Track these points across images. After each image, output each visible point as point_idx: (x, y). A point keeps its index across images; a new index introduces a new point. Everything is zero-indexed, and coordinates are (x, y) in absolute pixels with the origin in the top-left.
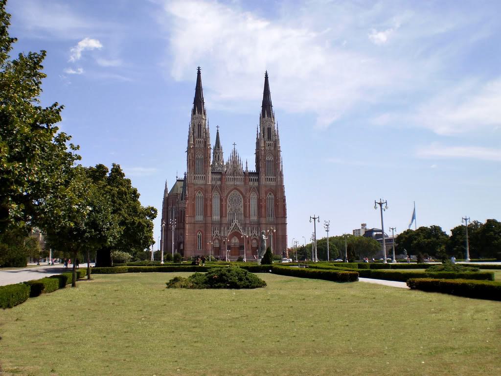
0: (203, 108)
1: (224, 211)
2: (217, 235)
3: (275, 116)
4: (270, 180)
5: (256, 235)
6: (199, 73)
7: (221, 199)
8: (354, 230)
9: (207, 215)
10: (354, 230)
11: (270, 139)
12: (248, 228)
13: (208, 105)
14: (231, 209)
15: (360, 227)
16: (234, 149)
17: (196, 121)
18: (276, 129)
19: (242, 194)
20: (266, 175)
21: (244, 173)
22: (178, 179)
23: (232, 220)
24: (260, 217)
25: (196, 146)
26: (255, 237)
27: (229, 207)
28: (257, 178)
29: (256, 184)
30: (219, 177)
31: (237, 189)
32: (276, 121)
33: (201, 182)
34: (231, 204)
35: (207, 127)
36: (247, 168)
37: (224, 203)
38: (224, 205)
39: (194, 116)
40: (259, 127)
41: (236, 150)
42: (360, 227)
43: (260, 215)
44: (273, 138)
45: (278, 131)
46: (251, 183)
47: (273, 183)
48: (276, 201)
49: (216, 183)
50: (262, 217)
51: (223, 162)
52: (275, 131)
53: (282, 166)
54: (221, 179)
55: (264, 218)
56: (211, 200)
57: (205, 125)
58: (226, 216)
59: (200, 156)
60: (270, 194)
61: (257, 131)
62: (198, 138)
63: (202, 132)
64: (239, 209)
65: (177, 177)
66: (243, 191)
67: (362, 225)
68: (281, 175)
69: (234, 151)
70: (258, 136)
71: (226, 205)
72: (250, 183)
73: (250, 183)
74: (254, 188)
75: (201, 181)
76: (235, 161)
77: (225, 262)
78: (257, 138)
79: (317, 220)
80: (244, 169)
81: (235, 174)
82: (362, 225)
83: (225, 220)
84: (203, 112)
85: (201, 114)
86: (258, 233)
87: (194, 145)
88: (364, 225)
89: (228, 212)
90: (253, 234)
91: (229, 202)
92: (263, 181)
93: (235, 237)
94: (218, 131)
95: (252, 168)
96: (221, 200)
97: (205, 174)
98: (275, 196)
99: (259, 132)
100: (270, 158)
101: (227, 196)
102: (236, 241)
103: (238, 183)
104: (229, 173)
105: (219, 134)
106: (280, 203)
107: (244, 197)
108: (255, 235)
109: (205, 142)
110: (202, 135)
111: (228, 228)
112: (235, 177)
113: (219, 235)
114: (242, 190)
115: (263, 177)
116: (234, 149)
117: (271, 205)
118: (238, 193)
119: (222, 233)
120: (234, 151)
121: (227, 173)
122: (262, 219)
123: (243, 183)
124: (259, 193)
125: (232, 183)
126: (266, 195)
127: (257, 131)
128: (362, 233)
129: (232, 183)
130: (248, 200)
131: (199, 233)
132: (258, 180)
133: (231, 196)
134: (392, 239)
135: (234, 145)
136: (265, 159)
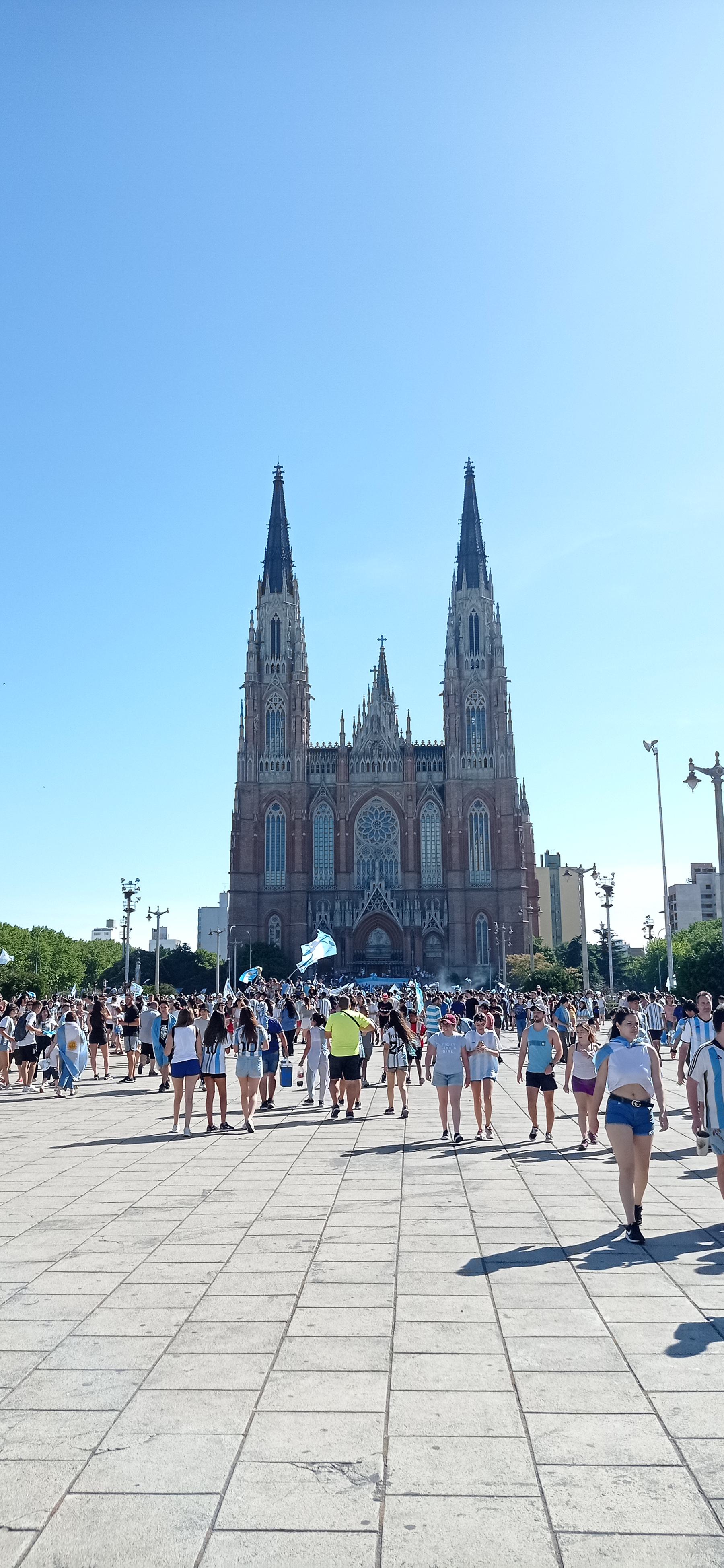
0: (482, 576)
3: (494, 582)
5: (438, 922)
6: (278, 482)
9: (293, 868)
10: (200, 910)
14: (365, 851)
17: (269, 611)
24: (447, 871)
26: (432, 929)
27: (359, 843)
36: (409, 732)
37: (343, 834)
39: (459, 592)
40: (255, 612)
44: (484, 644)
46: (423, 776)
47: (486, 773)
49: (430, 777)
50: (451, 870)
55: (458, 873)
62: (273, 656)
63: (283, 641)
66: (397, 799)
68: (509, 748)
72: (418, 774)
84: (482, 581)
85: (477, 586)
86: (442, 917)
90: (427, 920)
93: (378, 929)
97: (491, 751)
98: (493, 808)
101: (353, 814)
102: (382, 942)
103: (384, 776)
106: (504, 829)
107: (402, 815)
108: (433, 922)
109: (291, 668)
110: (282, 647)
111: (355, 905)
118: (384, 803)
119: (337, 917)
122: (451, 875)
123: (398, 776)
124: (443, 799)
125: (368, 776)
129: (368, 776)
131: (482, 917)
132: (443, 768)
133: (365, 813)
136: (462, 704)
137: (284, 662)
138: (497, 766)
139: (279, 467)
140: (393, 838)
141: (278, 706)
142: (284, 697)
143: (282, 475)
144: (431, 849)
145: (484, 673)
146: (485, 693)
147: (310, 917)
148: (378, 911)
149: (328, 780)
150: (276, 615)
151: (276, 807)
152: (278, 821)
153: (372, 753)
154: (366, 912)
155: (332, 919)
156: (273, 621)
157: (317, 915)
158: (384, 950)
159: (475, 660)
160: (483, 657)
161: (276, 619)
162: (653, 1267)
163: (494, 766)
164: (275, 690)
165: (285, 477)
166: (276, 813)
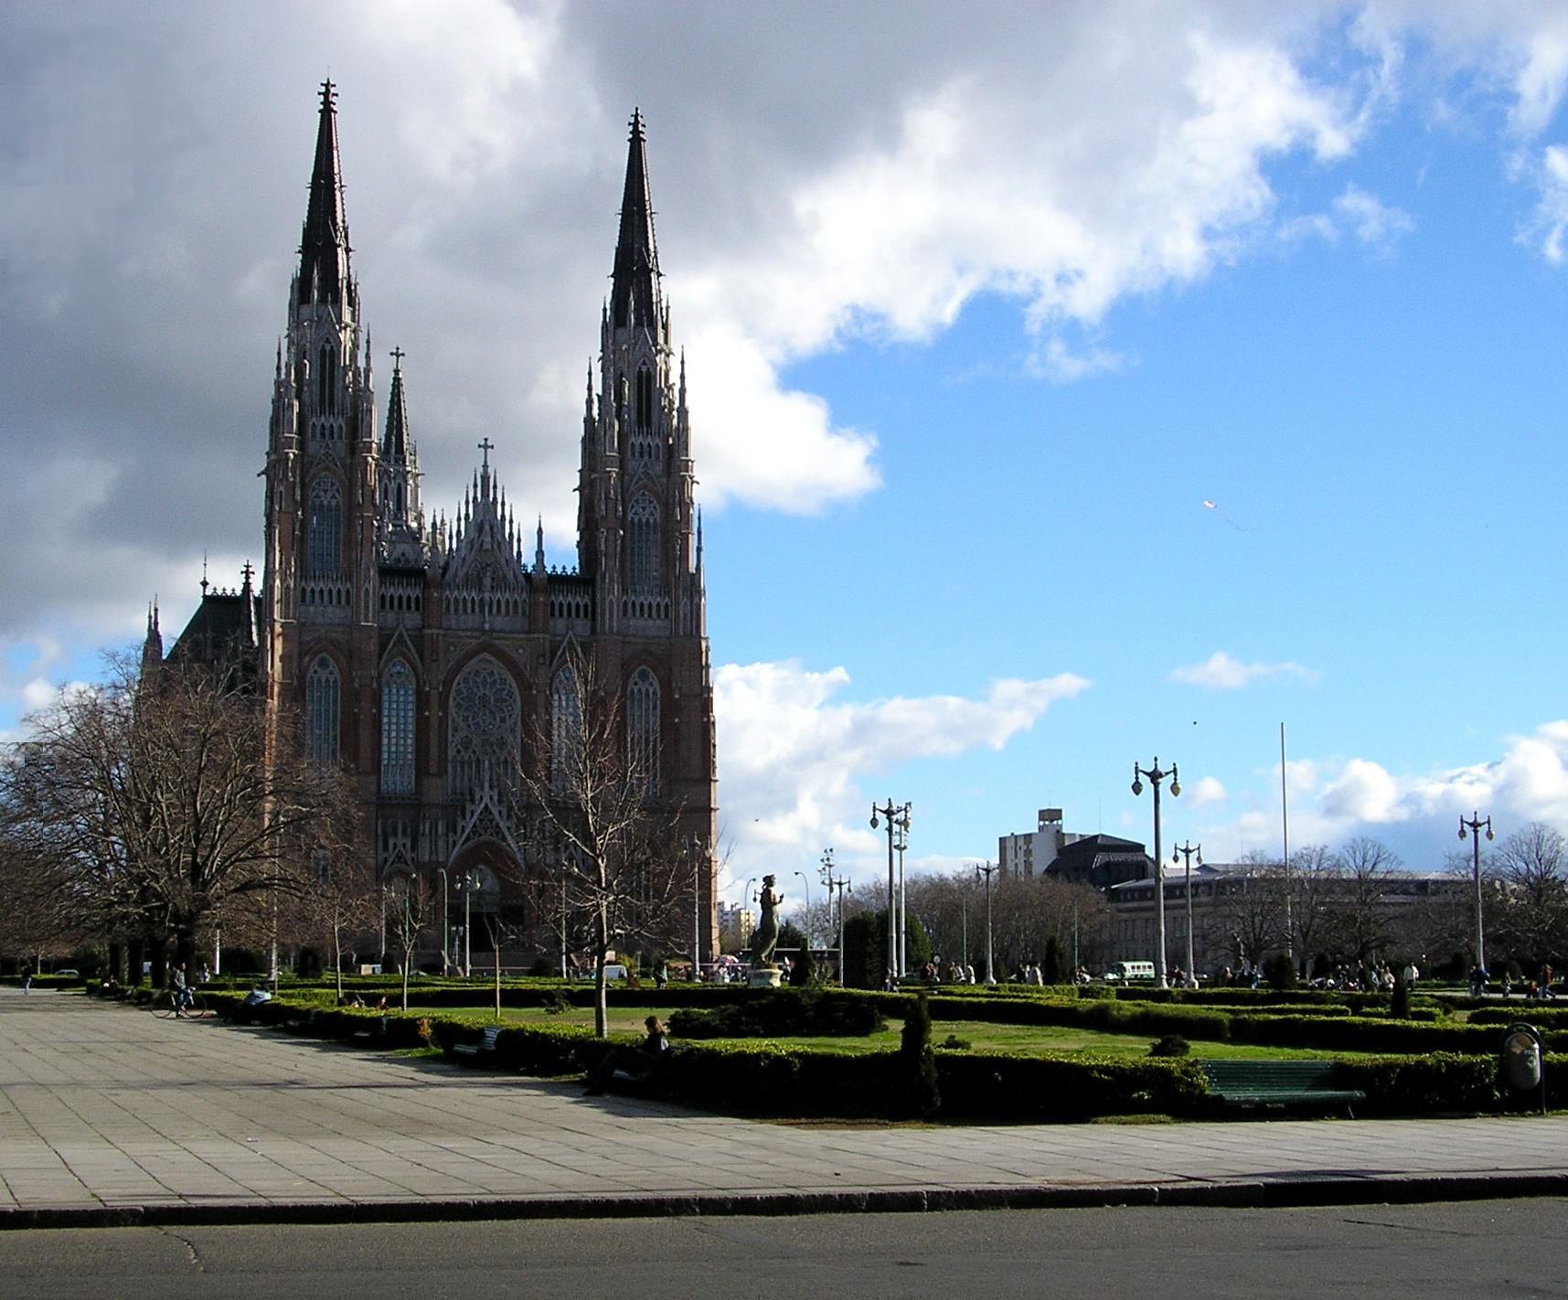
1: (434, 751)
2: (399, 857)
4: (647, 611)
6: (327, 112)
7: (419, 692)
8: (1002, 840)
10: (1002, 840)
11: (649, 425)
12: (434, 826)
13: (352, 264)
14: (466, 743)
15: (1031, 825)
16: (485, 466)
18: (674, 378)
19: (518, 675)
20: (624, 591)
21: (528, 576)
22: (208, 593)
23: (471, 793)
25: (312, 447)
27: (455, 730)
28: (587, 599)
29: (582, 626)
30: (414, 592)
31: (499, 653)
32: (674, 345)
33: (334, 614)
34: (466, 719)
35: (361, 363)
37: (434, 713)
38: (434, 722)
39: (305, 310)
41: (491, 471)
42: (1031, 825)
43: (422, 770)
45: (683, 391)
48: (670, 707)
51: (419, 517)
52: (670, 388)
53: (699, 549)
54: (420, 605)
56: (377, 700)
57: (354, 357)
58: (442, 772)
59: (329, 498)
60: (644, 676)
61: (590, 388)
64: (502, 743)
65: (205, 584)
67: (1043, 815)
68: (693, 587)
69: (485, 478)
70: (589, 409)
71: (443, 722)
73: (551, 623)
74: (400, 639)
75: (330, 609)
76: (486, 522)
77: (441, 984)
78: (589, 420)
79: (1165, 783)
80: (529, 560)
81: (487, 582)
82: (1043, 815)
83: (436, 792)
87: (302, 445)
88: (1051, 815)
89: (451, 753)
91: (459, 706)
92: (611, 619)
94: (397, 372)
95: (564, 550)
96: (422, 701)
98: (666, 683)
99: (598, 389)
100: (646, 512)
101: (448, 683)
104: (461, 574)
105: (403, 389)
107: (525, 686)
108: (399, 857)
112: (487, 596)
113: (408, 856)
114: (520, 655)
115: (611, 594)
116: (485, 466)
117: (645, 721)
118: (496, 666)
119: (425, 845)
120: (485, 478)
121: (451, 571)
125: (470, 620)
126: (626, 677)
127: (590, 388)
128: (1043, 858)
130: (541, 701)
132: (591, 612)
134: (1182, 887)
135: (486, 447)
137: (341, 421)
138: (677, 616)
139: (327, 85)
140: (509, 722)
141: (329, 494)
142: (341, 481)
143: (333, 99)
144: (397, 723)
145: (659, 468)
146: (659, 500)
147: (381, 845)
148: (486, 837)
149: (409, 624)
150: (328, 341)
151: (323, 663)
152: (327, 686)
153: (480, 579)
154: (468, 839)
155: (414, 848)
156: (323, 351)
157: (391, 842)
158: (489, 899)
159: (327, 425)
160: (341, 421)
161: (328, 348)
162: (25, 1208)
163: (672, 615)
164: (327, 468)
165: (338, 104)
166: (324, 675)
